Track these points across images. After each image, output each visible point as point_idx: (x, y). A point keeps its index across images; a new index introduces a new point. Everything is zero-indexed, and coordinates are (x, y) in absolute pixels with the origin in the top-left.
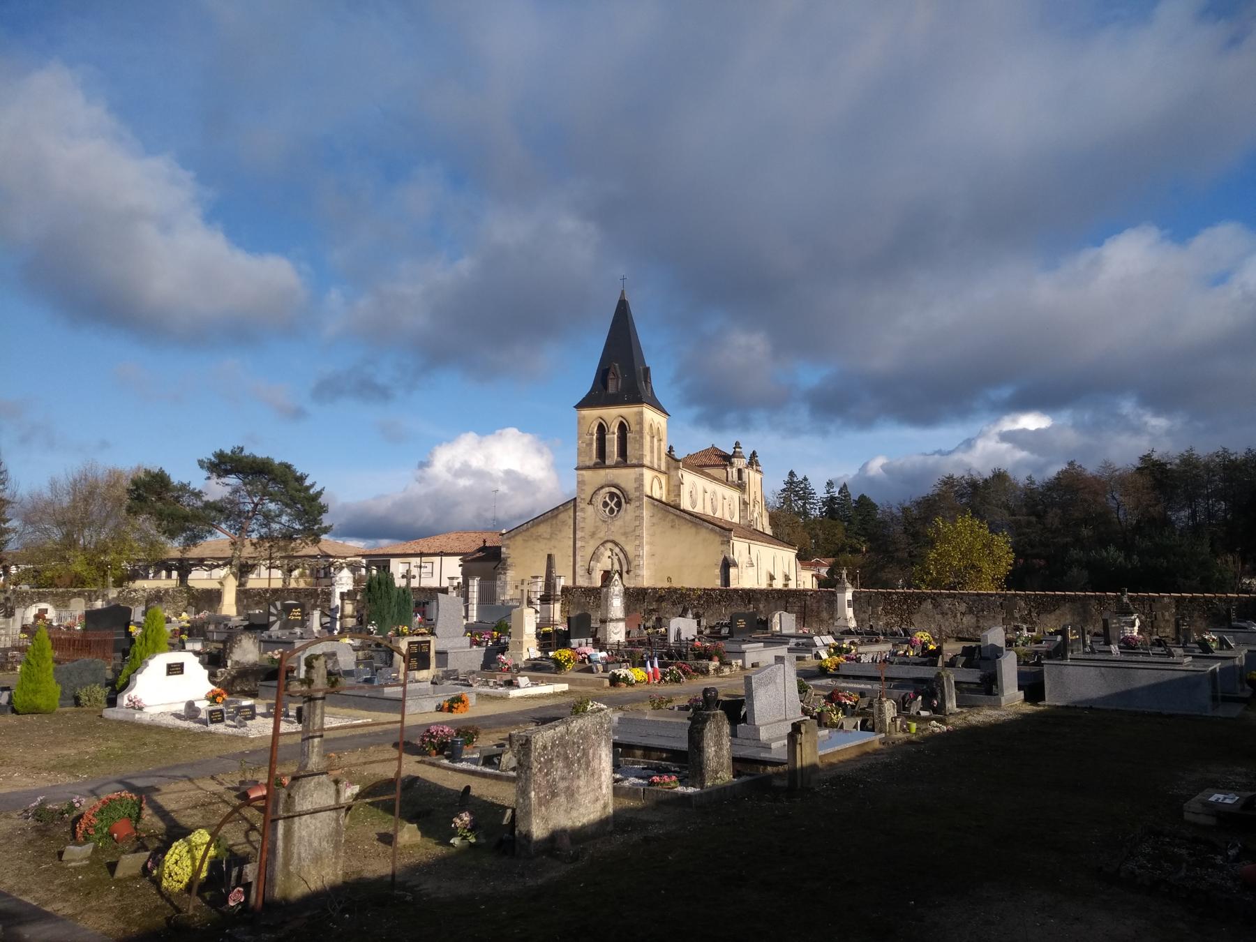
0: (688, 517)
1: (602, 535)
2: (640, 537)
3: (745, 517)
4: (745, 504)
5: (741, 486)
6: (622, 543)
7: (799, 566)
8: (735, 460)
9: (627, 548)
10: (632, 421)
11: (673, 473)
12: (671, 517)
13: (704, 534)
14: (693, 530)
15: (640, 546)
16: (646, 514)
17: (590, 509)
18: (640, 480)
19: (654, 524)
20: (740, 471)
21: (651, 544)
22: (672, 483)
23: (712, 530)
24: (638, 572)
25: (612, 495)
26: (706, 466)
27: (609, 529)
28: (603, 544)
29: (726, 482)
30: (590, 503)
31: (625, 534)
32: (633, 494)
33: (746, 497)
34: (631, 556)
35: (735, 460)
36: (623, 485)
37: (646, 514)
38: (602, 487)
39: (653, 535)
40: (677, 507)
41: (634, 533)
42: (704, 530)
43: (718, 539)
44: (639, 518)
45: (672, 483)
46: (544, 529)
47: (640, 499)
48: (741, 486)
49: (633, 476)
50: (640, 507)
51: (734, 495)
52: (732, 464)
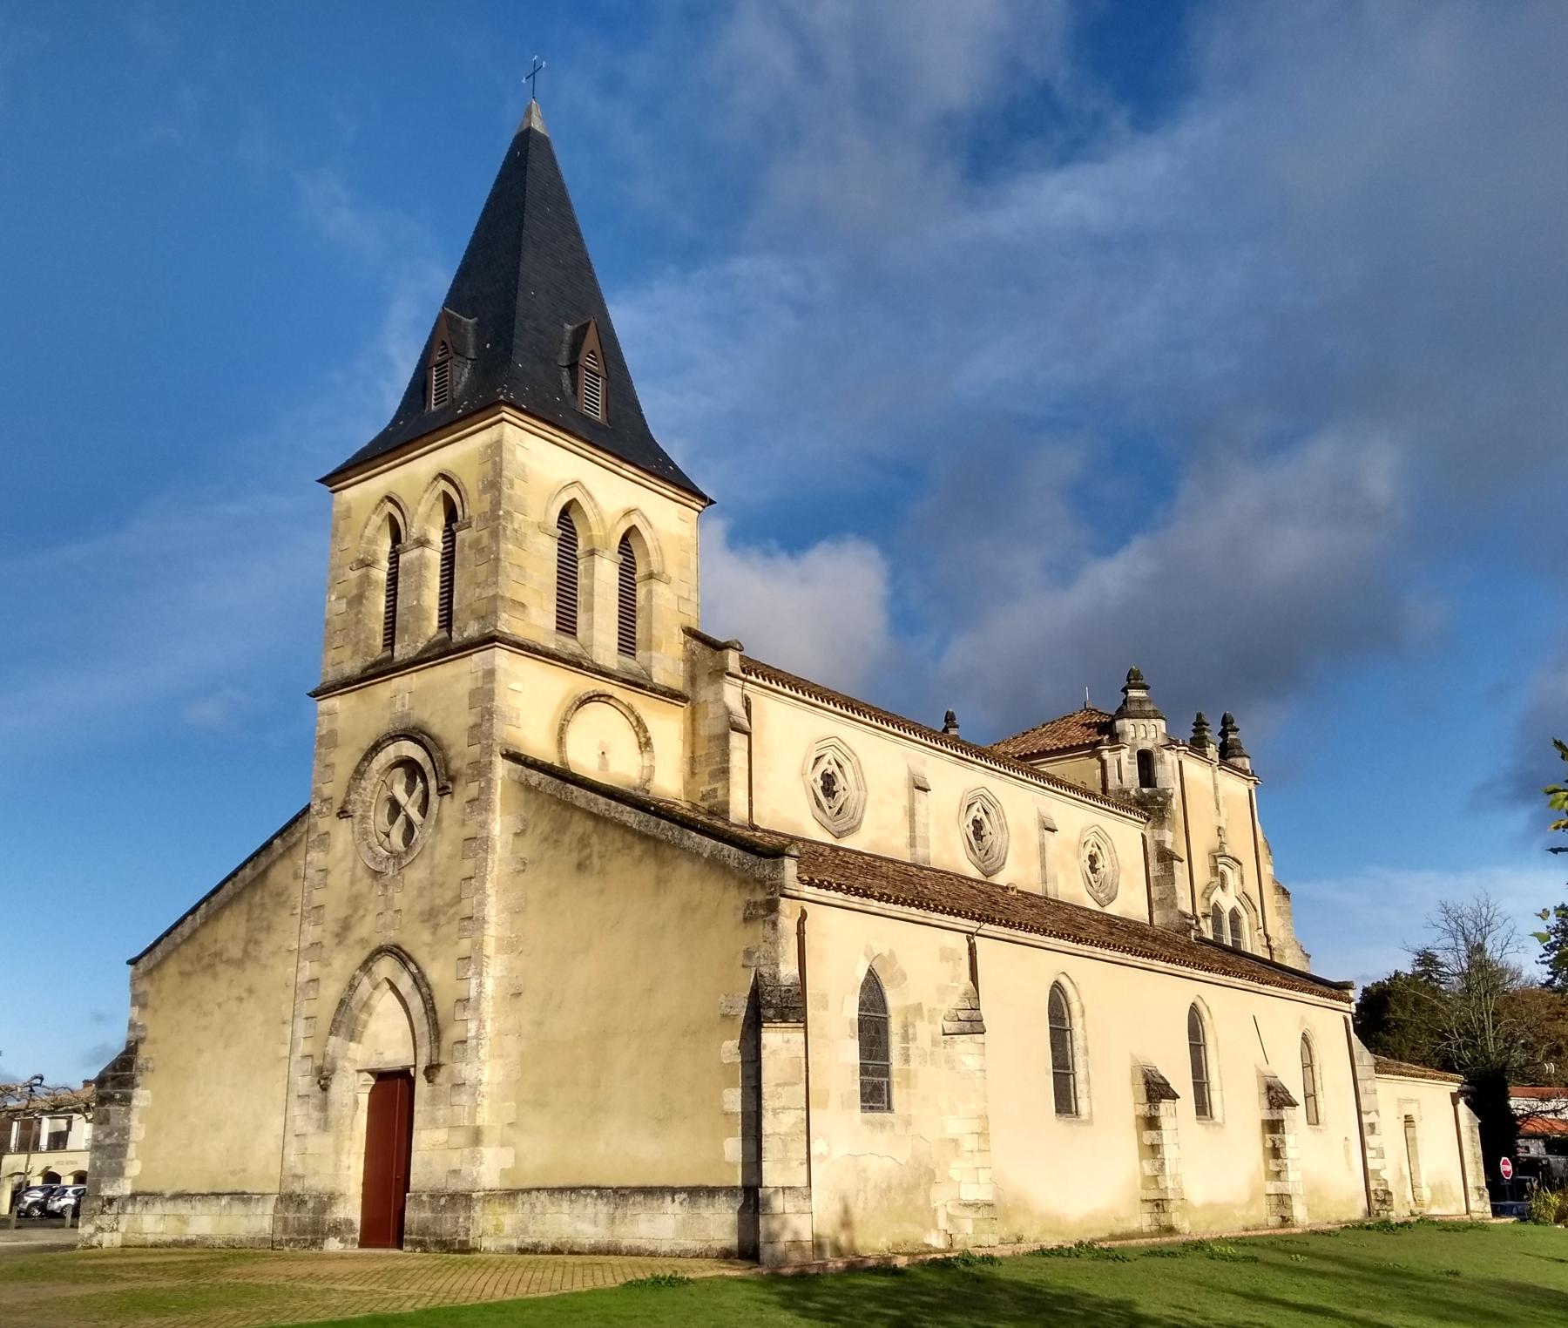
0: (630, 816)
1: (370, 930)
2: (473, 921)
3: (1169, 902)
4: (1166, 857)
5: (1149, 803)
6: (421, 955)
7: (1366, 1058)
8: (1126, 725)
9: (436, 973)
10: (471, 481)
11: (706, 693)
12: (580, 826)
13: (686, 881)
14: (649, 870)
15: (470, 961)
16: (500, 825)
17: (343, 834)
18: (484, 696)
19: (524, 865)
20: (1146, 761)
21: (511, 946)
22: (704, 730)
23: (714, 862)
24: (467, 1071)
25: (409, 765)
26: (1043, 754)
27: (388, 902)
28: (366, 966)
29: (1103, 795)
30: (343, 813)
31: (431, 917)
32: (461, 753)
33: (1171, 838)
34: (443, 1004)
35: (1126, 725)
36: (436, 727)
37: (500, 825)
38: (376, 748)
39: (517, 911)
40: (1236, 951)
41: (453, 913)
42: (685, 868)
43: (733, 900)
44: (476, 844)
45: (704, 730)
46: (230, 930)
47: (481, 770)
48: (1149, 803)
49: (465, 686)
50: (479, 803)
51: (1126, 838)
52: (1115, 738)
